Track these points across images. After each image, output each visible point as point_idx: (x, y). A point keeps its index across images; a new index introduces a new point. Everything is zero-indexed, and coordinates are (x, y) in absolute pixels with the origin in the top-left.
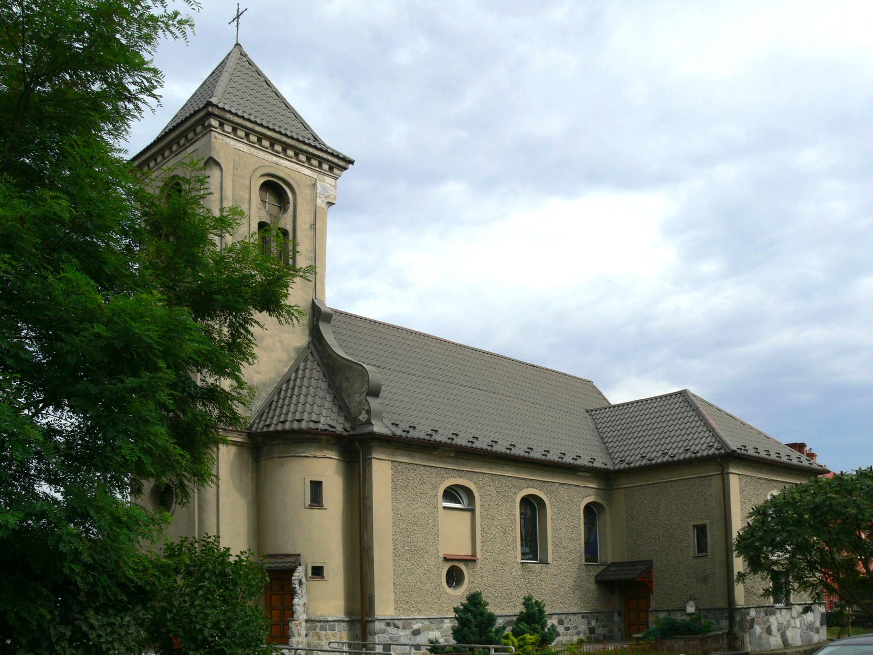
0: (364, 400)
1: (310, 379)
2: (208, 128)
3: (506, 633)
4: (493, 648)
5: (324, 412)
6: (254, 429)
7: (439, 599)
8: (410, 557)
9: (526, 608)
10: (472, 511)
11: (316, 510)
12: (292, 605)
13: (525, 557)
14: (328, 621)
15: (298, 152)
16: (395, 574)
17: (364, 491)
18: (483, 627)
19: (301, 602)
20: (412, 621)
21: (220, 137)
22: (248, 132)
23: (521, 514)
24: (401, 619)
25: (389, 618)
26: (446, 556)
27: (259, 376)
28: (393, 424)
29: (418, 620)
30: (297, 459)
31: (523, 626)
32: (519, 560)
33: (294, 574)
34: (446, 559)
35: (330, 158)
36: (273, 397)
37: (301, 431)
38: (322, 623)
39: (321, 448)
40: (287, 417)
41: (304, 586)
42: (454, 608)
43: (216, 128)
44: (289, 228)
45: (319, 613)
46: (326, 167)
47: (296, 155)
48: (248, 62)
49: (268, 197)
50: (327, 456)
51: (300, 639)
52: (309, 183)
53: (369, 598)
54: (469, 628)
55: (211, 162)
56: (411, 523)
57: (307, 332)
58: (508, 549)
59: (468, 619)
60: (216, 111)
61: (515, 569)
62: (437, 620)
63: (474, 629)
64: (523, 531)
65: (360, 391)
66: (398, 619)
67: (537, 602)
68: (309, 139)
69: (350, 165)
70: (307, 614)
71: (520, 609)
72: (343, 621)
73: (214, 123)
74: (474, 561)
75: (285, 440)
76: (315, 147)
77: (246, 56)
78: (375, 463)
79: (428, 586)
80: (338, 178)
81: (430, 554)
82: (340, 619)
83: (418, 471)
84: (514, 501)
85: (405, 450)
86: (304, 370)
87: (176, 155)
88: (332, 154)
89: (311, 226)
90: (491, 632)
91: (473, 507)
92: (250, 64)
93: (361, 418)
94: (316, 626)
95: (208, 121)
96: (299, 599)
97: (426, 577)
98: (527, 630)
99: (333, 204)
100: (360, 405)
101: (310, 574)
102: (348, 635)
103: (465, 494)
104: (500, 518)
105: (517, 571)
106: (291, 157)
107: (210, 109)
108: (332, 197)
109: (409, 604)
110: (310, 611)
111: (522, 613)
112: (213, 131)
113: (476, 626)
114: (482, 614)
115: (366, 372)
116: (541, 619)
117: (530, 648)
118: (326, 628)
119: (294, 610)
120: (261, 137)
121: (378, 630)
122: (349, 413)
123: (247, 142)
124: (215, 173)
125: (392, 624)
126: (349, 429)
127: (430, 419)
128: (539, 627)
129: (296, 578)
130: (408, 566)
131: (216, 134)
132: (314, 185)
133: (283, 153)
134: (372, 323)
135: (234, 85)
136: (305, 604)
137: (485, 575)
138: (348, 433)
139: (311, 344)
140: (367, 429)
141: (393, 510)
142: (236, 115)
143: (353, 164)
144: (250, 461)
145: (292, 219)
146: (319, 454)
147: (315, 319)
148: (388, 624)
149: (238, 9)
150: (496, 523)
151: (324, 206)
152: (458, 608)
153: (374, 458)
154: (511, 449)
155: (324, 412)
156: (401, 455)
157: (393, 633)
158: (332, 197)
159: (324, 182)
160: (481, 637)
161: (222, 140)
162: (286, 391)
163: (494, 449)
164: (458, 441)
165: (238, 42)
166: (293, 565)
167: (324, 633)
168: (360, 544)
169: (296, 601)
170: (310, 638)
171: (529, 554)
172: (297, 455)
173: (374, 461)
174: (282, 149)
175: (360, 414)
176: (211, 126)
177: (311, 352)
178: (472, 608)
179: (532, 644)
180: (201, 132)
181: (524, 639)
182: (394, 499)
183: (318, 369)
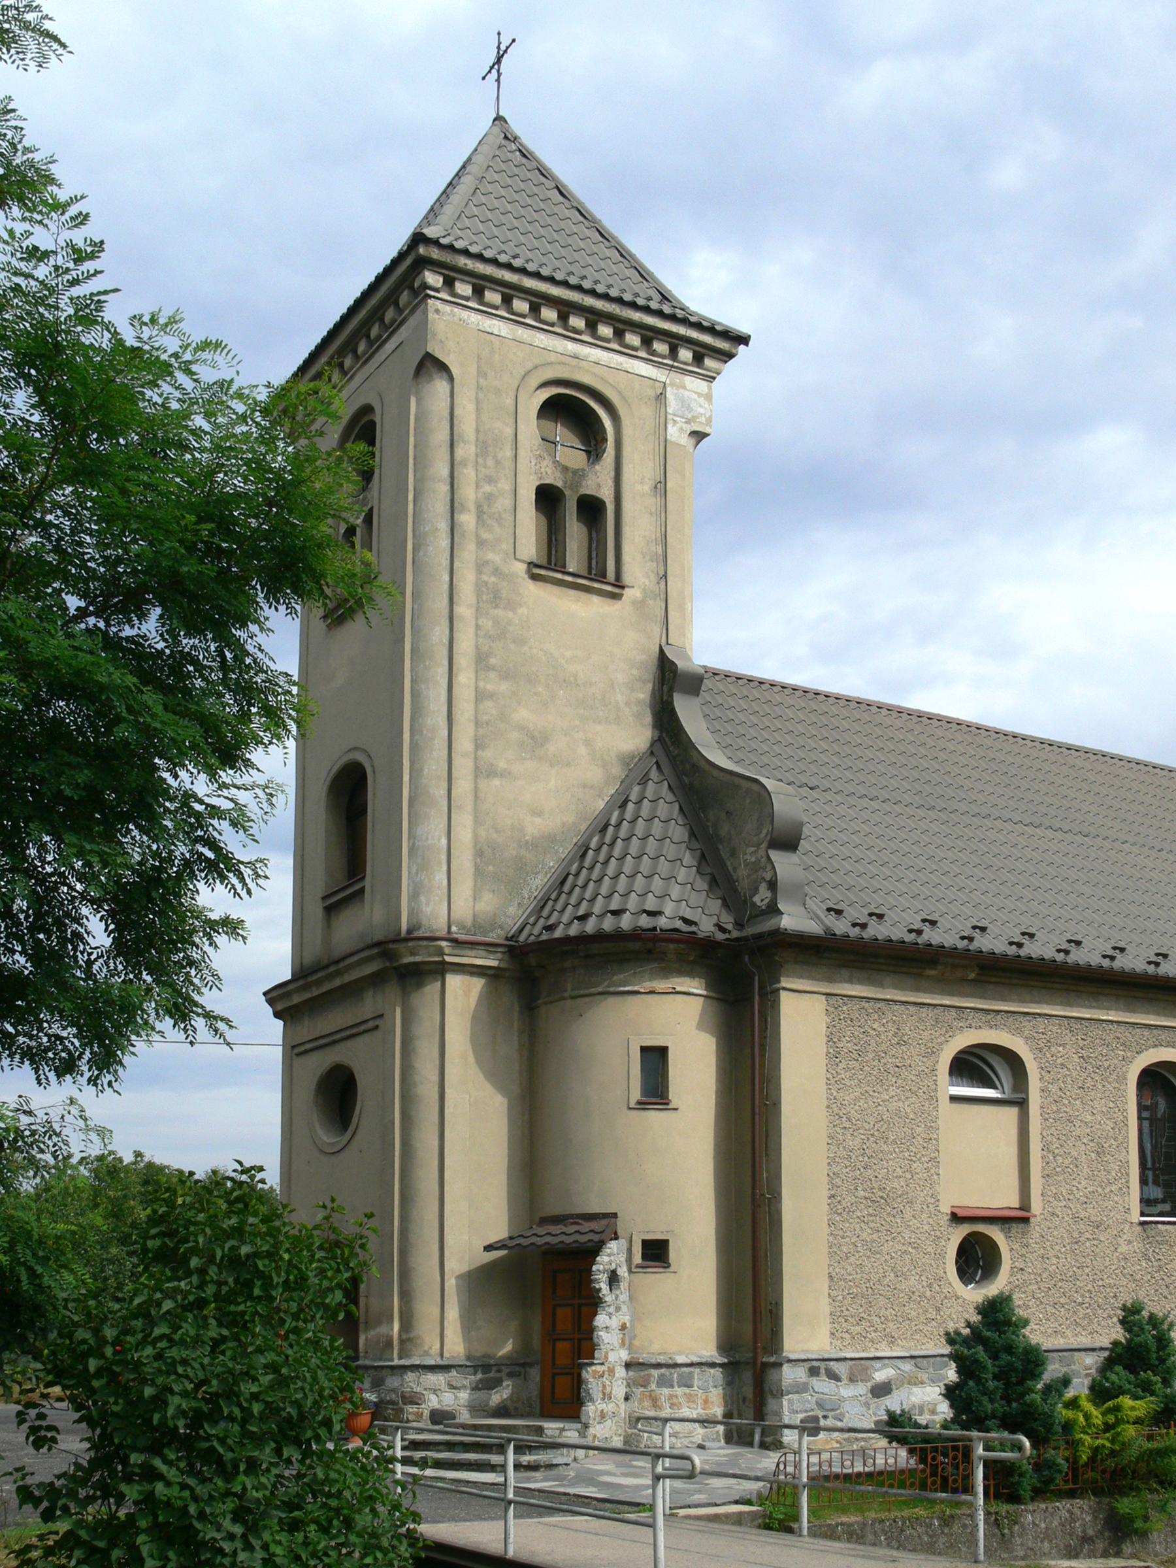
0: (764, 860)
1: (649, 820)
2: (421, 293)
3: (1070, 1393)
4: (980, 1439)
5: (675, 891)
6: (522, 938)
7: (938, 1310)
8: (870, 1215)
9: (1129, 1330)
10: (1022, 1104)
11: (653, 1113)
12: (591, 1330)
13: (1147, 1210)
14: (676, 1365)
15: (621, 327)
16: (832, 1254)
17: (762, 1066)
18: (1014, 1380)
19: (614, 1323)
20: (872, 1362)
21: (448, 308)
22: (509, 293)
23: (1141, 1108)
24: (845, 1359)
25: (814, 1357)
26: (956, 1210)
27: (538, 820)
28: (829, 910)
29: (886, 1361)
30: (612, 1000)
31: (1119, 1375)
32: (1136, 1217)
33: (598, 1259)
34: (956, 1218)
35: (694, 334)
36: (570, 864)
37: (618, 936)
38: (663, 1370)
39: (666, 972)
40: (592, 907)
41: (623, 1285)
42: (947, 1334)
43: (437, 290)
44: (606, 494)
45: (656, 1347)
46: (685, 354)
47: (619, 334)
48: (520, 151)
49: (561, 433)
50: (678, 989)
51: (609, 1407)
52: (651, 393)
53: (771, 1311)
54: (979, 1381)
55: (428, 364)
56: (873, 1135)
57: (648, 719)
58: (1107, 1190)
59: (976, 1361)
60: (435, 254)
61: (1125, 1237)
62: (932, 1360)
63: (991, 1384)
64: (1148, 1147)
65: (755, 839)
66: (837, 1360)
67: (1152, 1317)
68: (649, 299)
69: (742, 347)
70: (629, 1349)
71: (1111, 1333)
72: (713, 1365)
73: (432, 278)
74: (1026, 1220)
75: (587, 957)
76: (660, 314)
77: (516, 139)
78: (787, 1003)
79: (913, 1281)
80: (714, 378)
81: (918, 1207)
82: (703, 1360)
83: (889, 1015)
84: (1122, 1079)
85: (858, 968)
86: (639, 802)
87: (365, 363)
88: (698, 326)
89: (656, 487)
90: (1031, 1390)
91: (1023, 1096)
92: (524, 156)
93: (757, 899)
94: (649, 1376)
95: (421, 276)
96: (610, 1315)
97: (908, 1261)
98: (1128, 1386)
99: (705, 435)
100: (756, 871)
101: (637, 1258)
102: (725, 1396)
103: (1006, 1066)
104: (1089, 1118)
105: (1130, 1242)
106: (608, 340)
107: (422, 250)
108: (703, 420)
109: (865, 1324)
110: (636, 1343)
111: (1115, 1343)
112: (430, 297)
113: (996, 1377)
114: (1011, 1347)
115: (766, 794)
116: (1162, 1361)
117: (1130, 1431)
118: (671, 1380)
119: (596, 1340)
120: (537, 301)
121: (790, 1385)
122: (735, 891)
123: (507, 315)
124: (440, 386)
125: (822, 1371)
126: (729, 927)
127: (922, 897)
128: (1158, 1378)
129: (601, 1267)
130: (864, 1235)
131: (438, 303)
132: (661, 397)
133: (560, 323)
134: (842, 703)
135: (483, 199)
136: (623, 1327)
137: (1051, 1253)
138: (727, 936)
139: (658, 744)
140: (769, 925)
141: (828, 1107)
142: (480, 257)
143: (747, 344)
144: (517, 1008)
145: (612, 474)
146: (661, 985)
147: (665, 688)
148: (814, 1372)
149: (500, 43)
150: (1078, 1132)
151: (685, 441)
152: (957, 1333)
153: (785, 989)
154: (1157, 964)
155: (675, 891)
156: (850, 981)
157: (826, 1391)
158: (703, 420)
159: (684, 388)
160: (1009, 1405)
161: (453, 314)
162: (598, 850)
163: (1117, 964)
164: (984, 943)
165: (501, 114)
166: (596, 1238)
167: (666, 1391)
168: (754, 1188)
169: (601, 1320)
170: (634, 1405)
171: (1163, 1201)
172: (612, 989)
173: (783, 994)
174: (586, 325)
175: (756, 890)
176: (425, 286)
177: (657, 763)
178: (989, 1334)
179: (1138, 1421)
180: (409, 303)
181: (1117, 1409)
182: (833, 1081)
183: (670, 797)
